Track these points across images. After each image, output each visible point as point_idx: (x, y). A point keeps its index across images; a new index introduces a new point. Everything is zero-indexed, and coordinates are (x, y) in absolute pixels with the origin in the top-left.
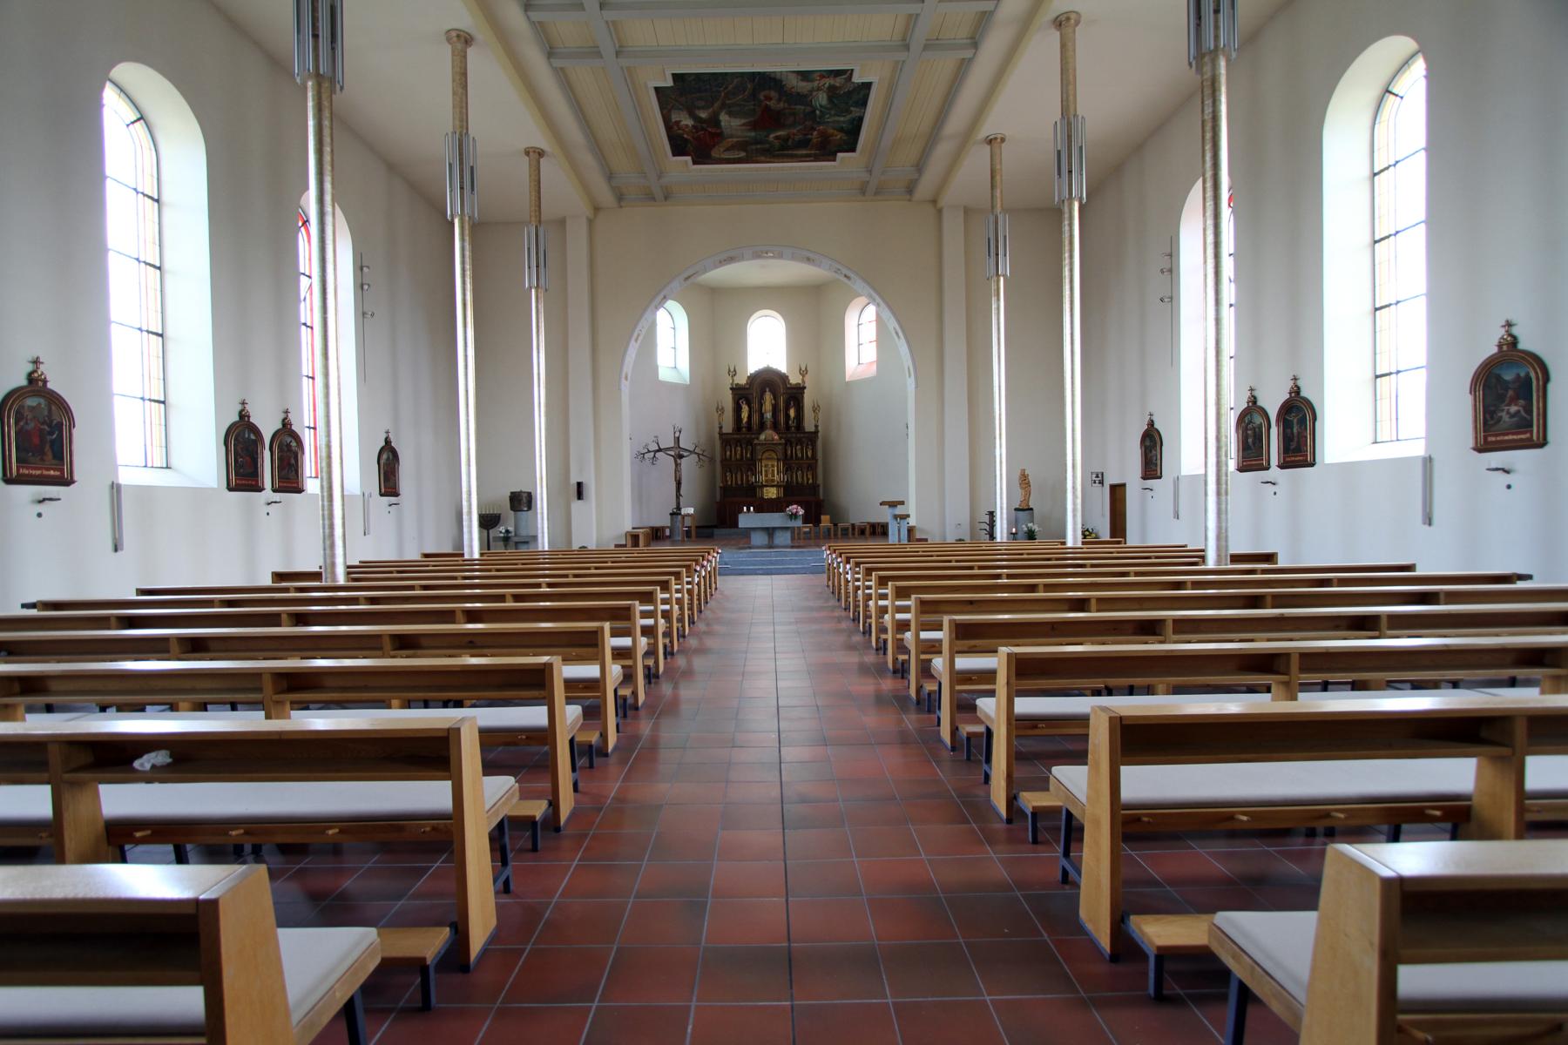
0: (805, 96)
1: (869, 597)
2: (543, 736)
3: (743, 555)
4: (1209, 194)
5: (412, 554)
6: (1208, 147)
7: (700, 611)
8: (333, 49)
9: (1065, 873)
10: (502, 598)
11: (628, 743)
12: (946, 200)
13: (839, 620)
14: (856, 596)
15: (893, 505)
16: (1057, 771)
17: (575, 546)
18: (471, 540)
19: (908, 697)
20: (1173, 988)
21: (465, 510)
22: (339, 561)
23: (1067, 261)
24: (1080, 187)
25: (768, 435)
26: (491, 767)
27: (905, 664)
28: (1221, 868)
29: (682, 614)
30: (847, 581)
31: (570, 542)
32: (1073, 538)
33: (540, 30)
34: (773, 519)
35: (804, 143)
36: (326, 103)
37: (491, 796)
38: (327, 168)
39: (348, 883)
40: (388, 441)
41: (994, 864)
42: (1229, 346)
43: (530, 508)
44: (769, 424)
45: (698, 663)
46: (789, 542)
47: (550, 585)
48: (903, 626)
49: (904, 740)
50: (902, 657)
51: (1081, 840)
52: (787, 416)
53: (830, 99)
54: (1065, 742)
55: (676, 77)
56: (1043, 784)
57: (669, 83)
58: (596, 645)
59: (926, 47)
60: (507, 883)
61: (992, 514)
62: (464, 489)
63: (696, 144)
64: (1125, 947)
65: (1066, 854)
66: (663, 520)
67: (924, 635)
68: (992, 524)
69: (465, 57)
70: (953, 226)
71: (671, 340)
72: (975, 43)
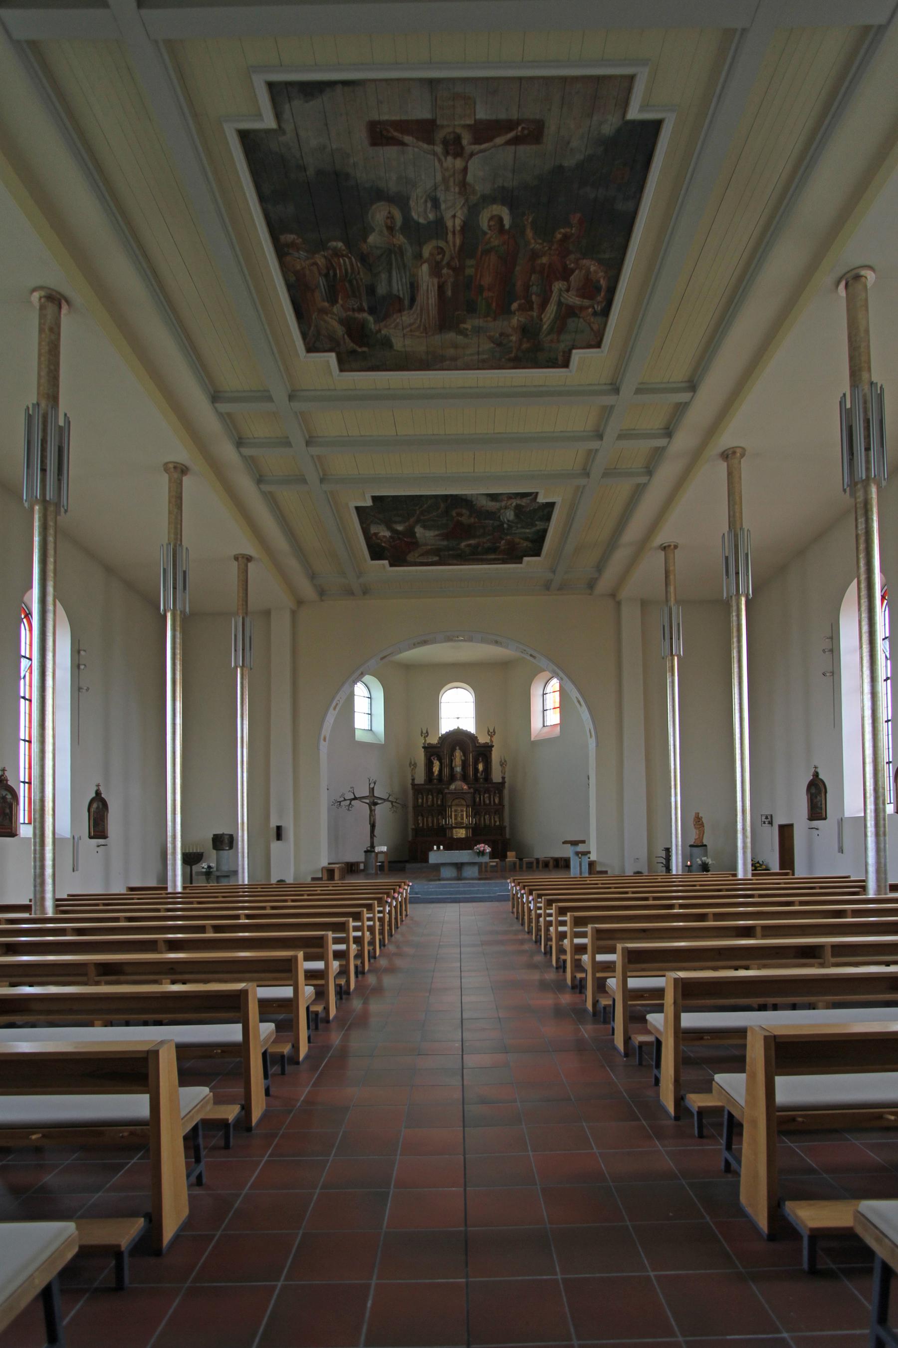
0: (494, 513)
1: (550, 924)
2: (240, 1050)
3: (432, 887)
4: (864, 593)
5: (119, 888)
6: (862, 556)
7: (391, 935)
8: (59, 480)
9: (728, 1164)
10: (202, 929)
11: (318, 1052)
12: (624, 594)
13: (522, 942)
14: (538, 922)
15: (575, 843)
16: (719, 1078)
17: (274, 881)
18: (175, 875)
19: (585, 1010)
20: (826, 1263)
21: (169, 851)
22: (49, 896)
23: (735, 645)
24: (747, 585)
25: (459, 785)
26: (187, 1077)
27: (583, 981)
28: (875, 1157)
29: (374, 939)
30: (530, 910)
31: (270, 880)
32: (743, 870)
33: (251, 464)
34: (463, 856)
35: (494, 550)
36: (51, 523)
37: (189, 1102)
38: (50, 574)
39: (48, 1178)
40: (98, 793)
41: (663, 1156)
42: (885, 711)
43: (231, 847)
44: (458, 776)
45: (388, 981)
46: (476, 874)
47: (248, 917)
48: (582, 949)
49: (580, 1047)
50: (579, 975)
51: (741, 1134)
52: (476, 770)
53: (517, 515)
54: (727, 1051)
55: (375, 499)
56: (706, 1087)
57: (369, 503)
58: (290, 971)
59: (605, 475)
60: (199, 1177)
61: (668, 850)
62: (169, 833)
63: (394, 551)
64: (782, 1228)
65: (729, 1147)
66: (357, 856)
67: (600, 958)
68: (668, 858)
69: (181, 484)
70: (631, 616)
71: (368, 709)
72: (649, 472)
